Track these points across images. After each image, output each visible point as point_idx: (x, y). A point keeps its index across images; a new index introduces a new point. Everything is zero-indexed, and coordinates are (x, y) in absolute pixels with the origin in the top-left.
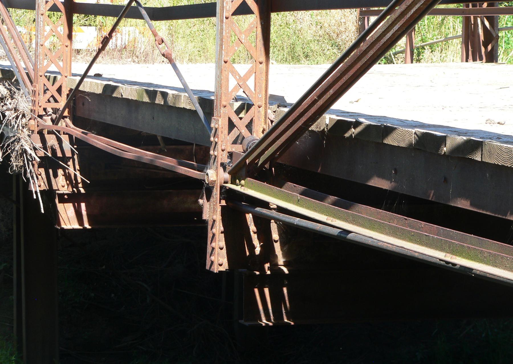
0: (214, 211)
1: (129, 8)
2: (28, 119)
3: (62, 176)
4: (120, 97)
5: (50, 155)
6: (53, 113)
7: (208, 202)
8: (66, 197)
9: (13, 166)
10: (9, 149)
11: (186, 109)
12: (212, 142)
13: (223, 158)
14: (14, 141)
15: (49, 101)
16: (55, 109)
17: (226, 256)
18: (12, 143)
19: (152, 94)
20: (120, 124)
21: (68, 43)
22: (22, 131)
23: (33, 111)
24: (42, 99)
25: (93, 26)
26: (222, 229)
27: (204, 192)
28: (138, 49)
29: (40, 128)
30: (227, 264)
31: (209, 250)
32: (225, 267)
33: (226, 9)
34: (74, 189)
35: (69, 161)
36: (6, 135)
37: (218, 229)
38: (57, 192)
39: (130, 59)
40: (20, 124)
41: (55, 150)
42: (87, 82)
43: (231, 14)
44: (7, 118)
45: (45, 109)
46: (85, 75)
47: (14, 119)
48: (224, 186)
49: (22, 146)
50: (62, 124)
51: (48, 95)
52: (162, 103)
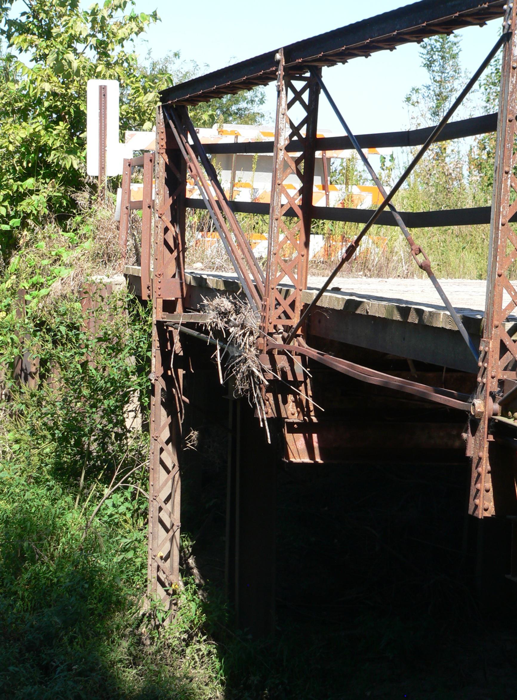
0: (480, 447)
1: (381, 213)
2: (256, 337)
3: (292, 403)
4: (365, 314)
5: (280, 379)
6: (284, 331)
7: (473, 436)
8: (295, 426)
9: (238, 390)
10: (234, 370)
11: (445, 329)
12: (480, 368)
13: (493, 386)
14: (240, 361)
15: (280, 317)
16: (286, 327)
17: (492, 500)
18: (237, 363)
19: (405, 311)
20: (364, 345)
21: (304, 252)
22: (249, 350)
23: (262, 328)
24: (273, 314)
25: (321, 234)
26: (489, 468)
27: (469, 425)
28: (371, 261)
29: (270, 347)
30: (494, 509)
31: (473, 492)
32: (491, 512)
33: (503, 214)
34: (306, 418)
35: (301, 386)
36: (231, 355)
37: (484, 469)
38: (286, 420)
39: (361, 273)
40: (247, 343)
41: (286, 372)
42: (326, 296)
43: (508, 220)
44: (232, 335)
45: (275, 327)
46: (324, 289)
47: (241, 337)
48: (492, 418)
49: (249, 367)
50: (294, 343)
51: (280, 310)
52: (417, 322)
